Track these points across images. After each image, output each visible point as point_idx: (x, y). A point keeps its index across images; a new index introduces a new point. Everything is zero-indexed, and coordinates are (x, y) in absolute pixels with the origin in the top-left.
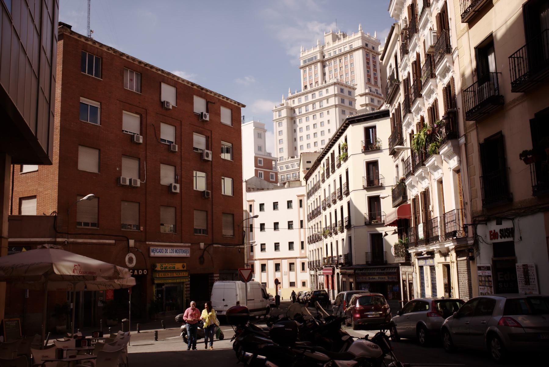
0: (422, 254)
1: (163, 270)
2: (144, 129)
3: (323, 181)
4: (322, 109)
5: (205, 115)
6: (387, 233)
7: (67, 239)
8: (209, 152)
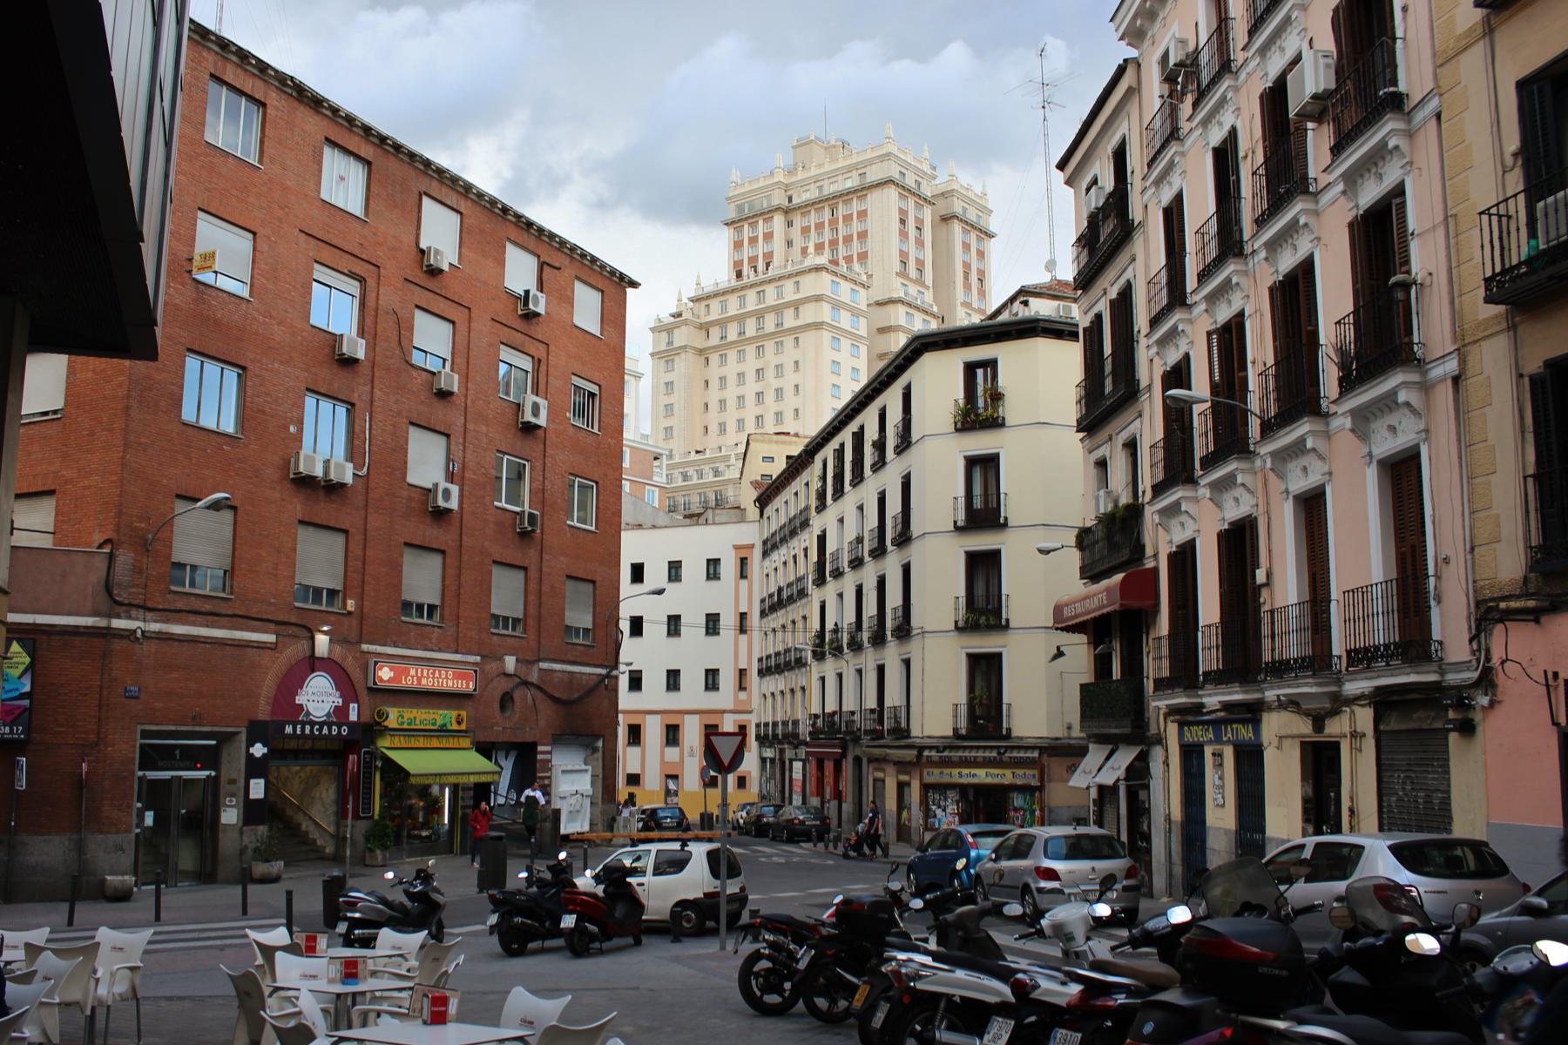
0: (1205, 710)
1: (405, 726)
2: (369, 321)
3: (822, 507)
4: (781, 331)
5: (535, 296)
6: (1062, 649)
7: (141, 624)
8: (542, 402)
